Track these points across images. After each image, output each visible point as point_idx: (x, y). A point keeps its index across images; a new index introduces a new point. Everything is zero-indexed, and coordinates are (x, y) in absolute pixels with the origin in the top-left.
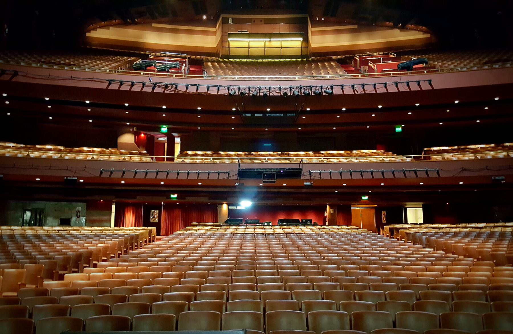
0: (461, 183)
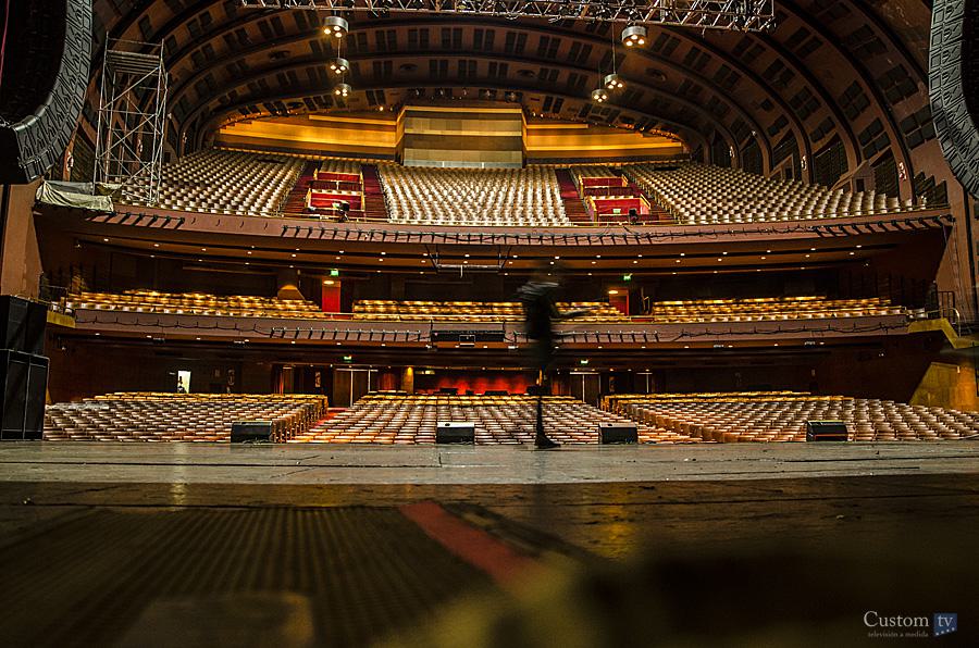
0: (410, 371)
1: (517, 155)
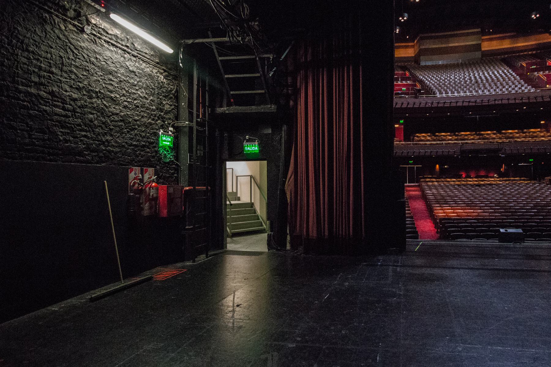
1: (478, 55)
